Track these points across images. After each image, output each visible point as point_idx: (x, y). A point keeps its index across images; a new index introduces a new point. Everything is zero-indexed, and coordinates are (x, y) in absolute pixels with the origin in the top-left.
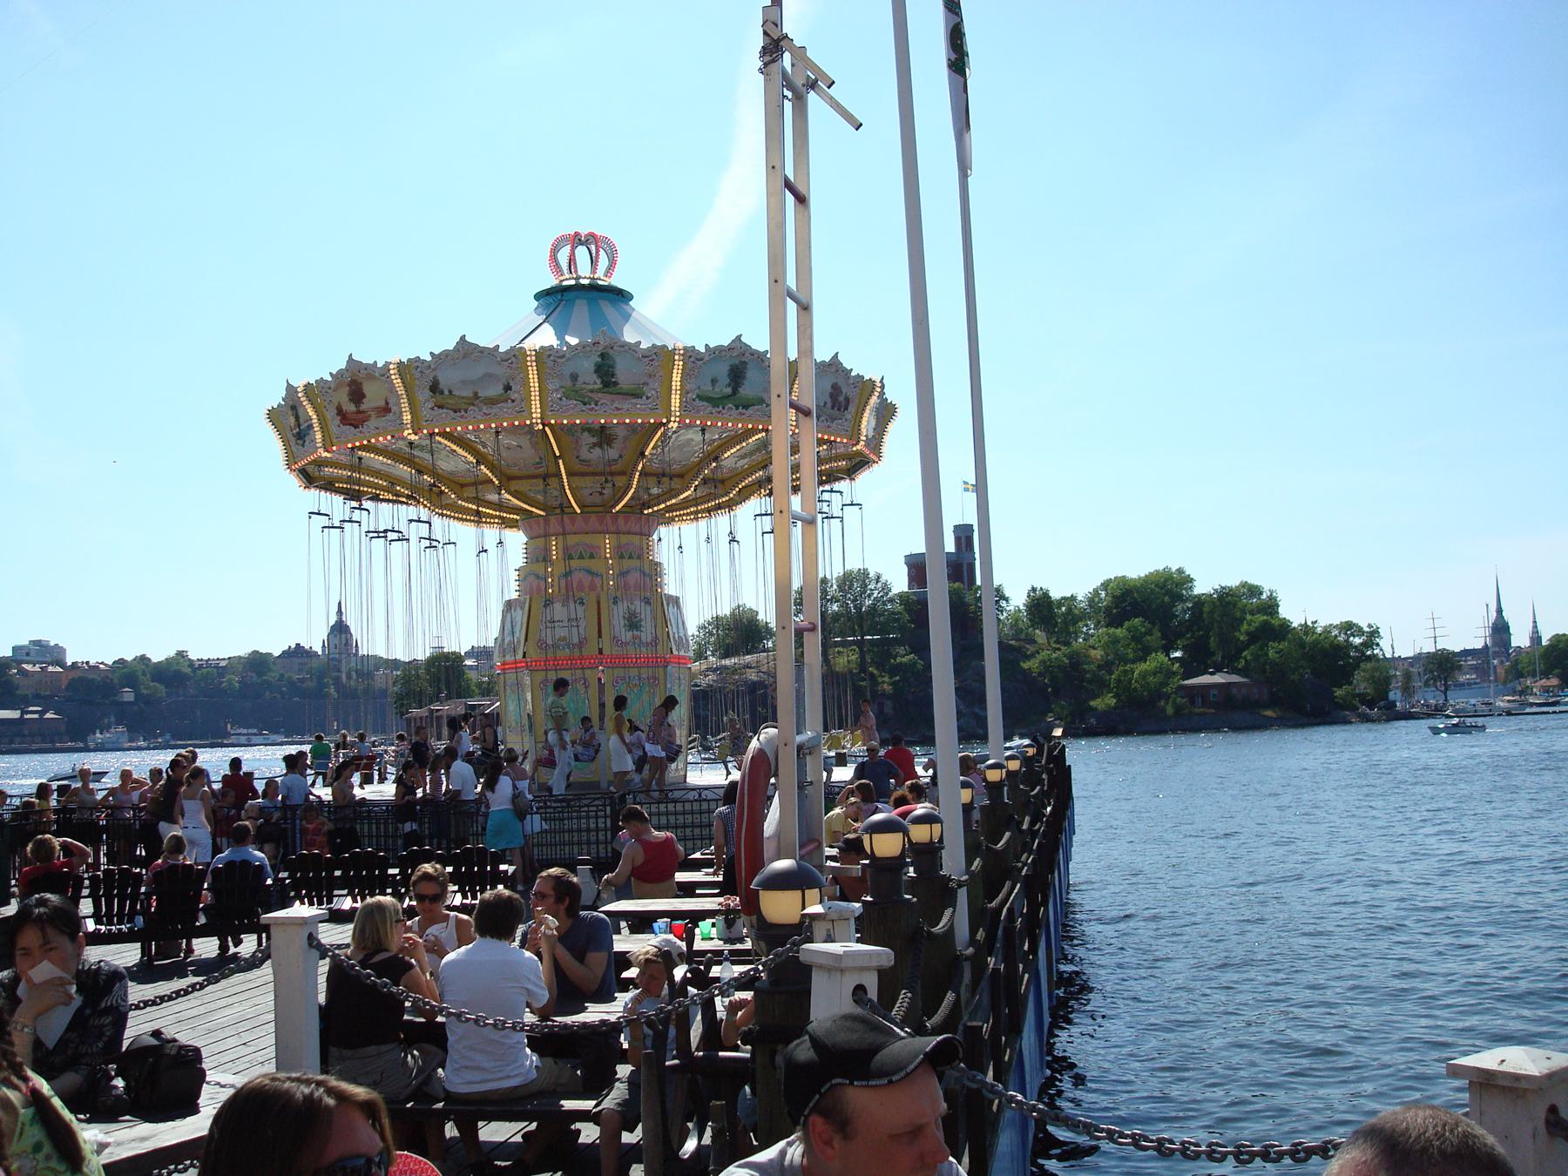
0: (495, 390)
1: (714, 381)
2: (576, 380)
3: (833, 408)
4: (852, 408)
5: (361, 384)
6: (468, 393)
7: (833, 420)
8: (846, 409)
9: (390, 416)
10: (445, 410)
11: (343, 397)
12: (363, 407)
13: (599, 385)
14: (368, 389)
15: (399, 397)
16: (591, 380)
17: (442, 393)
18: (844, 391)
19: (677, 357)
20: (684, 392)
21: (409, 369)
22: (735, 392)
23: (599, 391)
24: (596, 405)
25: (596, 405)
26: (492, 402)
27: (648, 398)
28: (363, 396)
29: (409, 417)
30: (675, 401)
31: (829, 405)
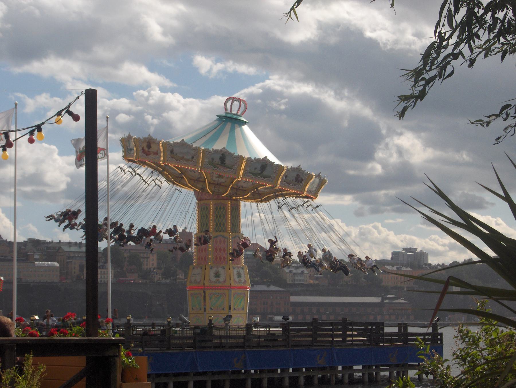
0: (189, 157)
1: (255, 169)
2: (213, 160)
3: (296, 182)
4: (303, 183)
5: (151, 143)
6: (181, 156)
7: (295, 185)
8: (301, 182)
9: (157, 156)
10: (173, 159)
11: (145, 145)
12: (150, 150)
13: (220, 163)
14: (153, 146)
15: (161, 152)
16: (217, 161)
17: (174, 153)
18: (301, 177)
19: (244, 160)
20: (245, 170)
21: (166, 145)
22: (262, 173)
23: (219, 165)
24: (218, 168)
25: (218, 168)
26: (187, 160)
27: (233, 170)
28: (151, 147)
29: (162, 158)
30: (241, 173)
31: (295, 180)
